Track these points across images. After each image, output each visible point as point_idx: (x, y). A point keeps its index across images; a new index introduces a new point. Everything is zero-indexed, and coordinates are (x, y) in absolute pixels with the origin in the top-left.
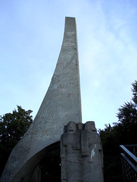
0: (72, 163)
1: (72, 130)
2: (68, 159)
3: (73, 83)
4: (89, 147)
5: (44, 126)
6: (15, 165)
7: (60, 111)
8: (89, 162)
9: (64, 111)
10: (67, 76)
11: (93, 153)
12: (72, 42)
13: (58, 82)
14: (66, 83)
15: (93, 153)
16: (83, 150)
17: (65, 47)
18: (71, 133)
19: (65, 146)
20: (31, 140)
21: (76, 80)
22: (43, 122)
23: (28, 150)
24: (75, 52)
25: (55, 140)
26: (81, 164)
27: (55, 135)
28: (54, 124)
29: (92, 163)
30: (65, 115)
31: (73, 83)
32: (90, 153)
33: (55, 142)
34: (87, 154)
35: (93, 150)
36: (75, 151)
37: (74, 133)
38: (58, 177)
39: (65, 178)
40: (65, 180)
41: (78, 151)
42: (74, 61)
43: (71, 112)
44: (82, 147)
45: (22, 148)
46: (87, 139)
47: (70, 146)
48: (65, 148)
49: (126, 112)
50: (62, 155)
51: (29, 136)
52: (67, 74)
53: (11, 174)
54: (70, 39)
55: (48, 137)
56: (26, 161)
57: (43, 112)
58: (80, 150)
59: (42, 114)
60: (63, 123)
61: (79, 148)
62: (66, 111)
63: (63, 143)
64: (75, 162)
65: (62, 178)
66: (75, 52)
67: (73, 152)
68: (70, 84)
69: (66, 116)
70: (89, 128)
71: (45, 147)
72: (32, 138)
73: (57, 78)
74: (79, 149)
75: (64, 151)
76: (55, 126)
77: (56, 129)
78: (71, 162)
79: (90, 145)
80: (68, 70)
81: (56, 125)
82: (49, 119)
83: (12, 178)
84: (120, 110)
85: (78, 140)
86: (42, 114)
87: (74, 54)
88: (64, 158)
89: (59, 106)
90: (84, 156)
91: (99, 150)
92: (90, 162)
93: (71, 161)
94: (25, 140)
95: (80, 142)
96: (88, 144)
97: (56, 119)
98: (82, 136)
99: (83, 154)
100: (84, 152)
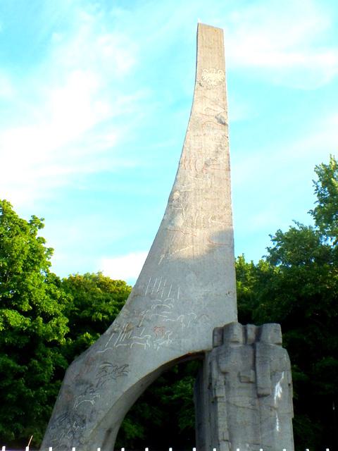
0: (239, 409)
1: (237, 342)
2: (232, 400)
3: (221, 218)
4: (271, 378)
5: (157, 317)
6: (92, 402)
7: (191, 285)
8: (271, 407)
9: (201, 284)
10: (206, 197)
11: (278, 392)
12: (215, 102)
13: (185, 210)
14: (203, 215)
15: (278, 392)
16: (260, 384)
17: (200, 116)
18: (234, 346)
19: (225, 373)
20: (128, 347)
21: (227, 211)
22: (154, 307)
23: (122, 370)
24: (223, 133)
25: (182, 349)
26: (256, 410)
27: (183, 340)
28: (179, 314)
29: (275, 409)
30: (203, 294)
31: (221, 218)
32: (273, 389)
33: (182, 354)
34: (265, 392)
35: (279, 383)
36: (245, 385)
37: (240, 347)
38: (189, 437)
39: (227, 436)
40: (227, 441)
41: (251, 385)
42: (222, 158)
43: (216, 290)
44: (259, 378)
45: (105, 363)
46: (268, 362)
47: (233, 375)
48: (223, 377)
49: (294, 244)
50: (221, 393)
51: (122, 337)
52: (207, 192)
53: (87, 421)
54: (211, 95)
55: (168, 342)
56: (121, 394)
57: (152, 282)
58: (255, 383)
59: (150, 288)
60: (199, 313)
61: (252, 380)
62: (206, 285)
63: (218, 367)
64: (244, 407)
65: (220, 438)
66: (223, 133)
67: (240, 387)
68: (214, 218)
69: (206, 297)
70: (269, 337)
71: (160, 365)
72: (128, 340)
73: (181, 198)
74: (250, 382)
75: (223, 384)
76: (181, 318)
77: (184, 325)
78: (237, 407)
79: (274, 375)
80: (209, 182)
81: (183, 316)
82: (169, 301)
83: (92, 431)
84: (280, 237)
85: (251, 362)
86: (150, 288)
87: (221, 137)
88: (223, 397)
89: (190, 273)
90: (261, 396)
91: (289, 385)
92: (272, 408)
93: (237, 404)
94: (105, 346)
95: (254, 368)
96: (269, 371)
97: (183, 303)
98: (258, 355)
99: (261, 392)
100: (262, 389)
